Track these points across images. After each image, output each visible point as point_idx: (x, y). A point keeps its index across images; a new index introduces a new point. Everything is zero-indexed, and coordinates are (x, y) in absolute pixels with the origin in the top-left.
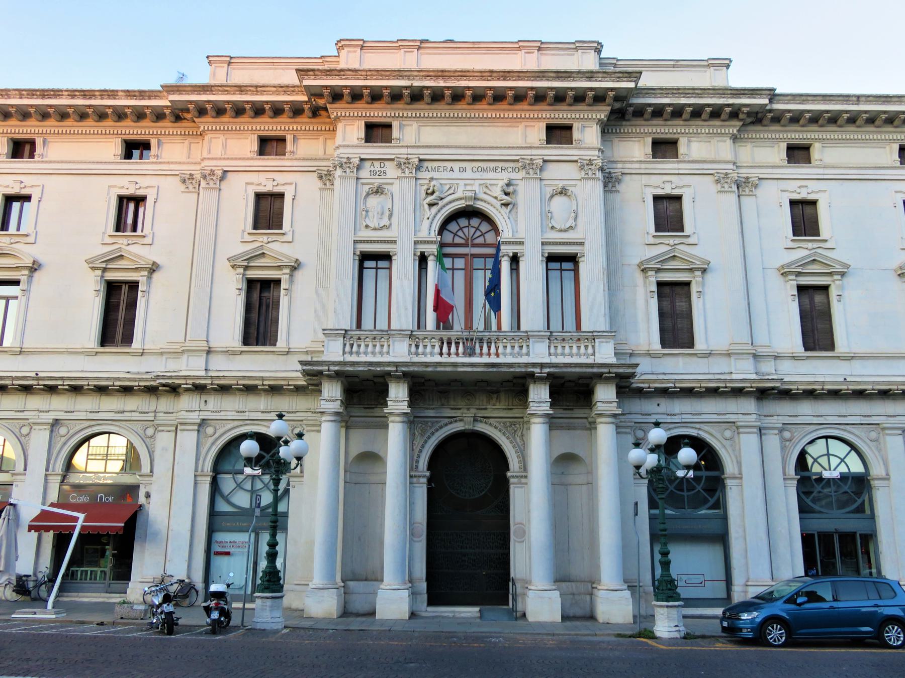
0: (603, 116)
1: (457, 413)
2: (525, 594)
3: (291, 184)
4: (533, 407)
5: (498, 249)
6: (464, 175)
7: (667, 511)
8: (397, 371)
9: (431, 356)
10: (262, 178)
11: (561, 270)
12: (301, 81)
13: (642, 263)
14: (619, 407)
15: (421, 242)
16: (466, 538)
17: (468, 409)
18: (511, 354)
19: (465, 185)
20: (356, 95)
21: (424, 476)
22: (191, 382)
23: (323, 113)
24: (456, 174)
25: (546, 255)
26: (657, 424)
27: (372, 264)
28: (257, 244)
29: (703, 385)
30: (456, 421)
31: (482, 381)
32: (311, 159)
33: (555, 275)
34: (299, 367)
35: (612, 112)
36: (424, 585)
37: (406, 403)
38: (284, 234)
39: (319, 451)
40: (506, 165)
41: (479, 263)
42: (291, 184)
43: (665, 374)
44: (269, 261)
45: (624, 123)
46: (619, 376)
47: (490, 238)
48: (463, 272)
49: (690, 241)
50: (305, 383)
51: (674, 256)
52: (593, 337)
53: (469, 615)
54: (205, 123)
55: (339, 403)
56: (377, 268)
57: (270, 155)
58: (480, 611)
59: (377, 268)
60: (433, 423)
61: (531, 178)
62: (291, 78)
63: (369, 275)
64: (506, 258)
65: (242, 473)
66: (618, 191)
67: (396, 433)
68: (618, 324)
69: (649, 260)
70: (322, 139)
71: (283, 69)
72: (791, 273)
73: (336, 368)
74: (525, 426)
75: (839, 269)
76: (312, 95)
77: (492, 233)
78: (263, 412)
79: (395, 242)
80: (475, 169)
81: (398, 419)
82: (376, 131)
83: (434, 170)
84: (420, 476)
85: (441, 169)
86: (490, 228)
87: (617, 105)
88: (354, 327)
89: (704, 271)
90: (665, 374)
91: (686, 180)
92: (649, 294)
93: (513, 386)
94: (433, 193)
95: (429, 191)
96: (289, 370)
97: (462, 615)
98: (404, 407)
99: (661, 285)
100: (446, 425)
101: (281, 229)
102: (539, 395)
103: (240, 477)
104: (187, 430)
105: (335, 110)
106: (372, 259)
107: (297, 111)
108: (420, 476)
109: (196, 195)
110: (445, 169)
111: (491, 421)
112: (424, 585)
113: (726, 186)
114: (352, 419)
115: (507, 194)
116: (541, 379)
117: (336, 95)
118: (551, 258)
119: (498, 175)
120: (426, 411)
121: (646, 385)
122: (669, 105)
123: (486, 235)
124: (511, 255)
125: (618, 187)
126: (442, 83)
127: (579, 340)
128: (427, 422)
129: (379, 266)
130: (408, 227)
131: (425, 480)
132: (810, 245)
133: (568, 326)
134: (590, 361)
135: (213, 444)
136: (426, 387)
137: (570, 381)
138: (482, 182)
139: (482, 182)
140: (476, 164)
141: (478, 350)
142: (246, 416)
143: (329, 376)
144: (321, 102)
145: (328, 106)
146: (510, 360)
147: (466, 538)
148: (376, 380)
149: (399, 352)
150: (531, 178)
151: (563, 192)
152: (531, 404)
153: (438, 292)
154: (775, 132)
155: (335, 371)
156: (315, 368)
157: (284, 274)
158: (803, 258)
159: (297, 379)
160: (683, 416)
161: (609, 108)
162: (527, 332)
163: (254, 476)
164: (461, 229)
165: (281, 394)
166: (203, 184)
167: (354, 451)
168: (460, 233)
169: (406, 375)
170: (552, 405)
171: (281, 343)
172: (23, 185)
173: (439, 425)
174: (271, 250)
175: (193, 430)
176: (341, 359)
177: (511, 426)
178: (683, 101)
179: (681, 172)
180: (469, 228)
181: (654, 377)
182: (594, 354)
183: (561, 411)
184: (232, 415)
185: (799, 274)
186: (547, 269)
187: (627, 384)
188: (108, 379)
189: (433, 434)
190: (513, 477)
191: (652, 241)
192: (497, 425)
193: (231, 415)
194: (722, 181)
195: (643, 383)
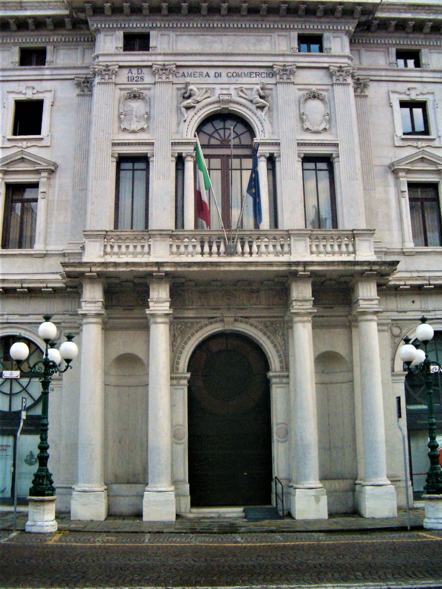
0: (351, 28)
2: (289, 494)
3: (51, 91)
4: (296, 307)
6: (219, 80)
7: (425, 407)
9: (192, 255)
10: (21, 87)
11: (316, 170)
13: (393, 164)
14: (379, 304)
15: (179, 143)
16: (232, 449)
19: (222, 89)
21: (185, 378)
23: (84, 27)
24: (212, 80)
25: (303, 155)
26: (423, 320)
27: (129, 166)
28: (15, 150)
30: (216, 322)
34: (61, 269)
35: (359, 25)
36: (187, 487)
37: (168, 304)
38: (42, 139)
39: (87, 351)
41: (235, 163)
42: (51, 91)
43: (418, 271)
44: (27, 165)
45: (370, 34)
47: (245, 139)
49: (436, 143)
50: (64, 285)
52: (353, 235)
53: (234, 515)
55: (100, 304)
56: (134, 170)
58: (244, 511)
59: (134, 170)
61: (285, 83)
63: (126, 176)
66: (366, 96)
69: (399, 162)
73: (99, 269)
74: (286, 325)
76: (73, 8)
77: (247, 135)
79: (152, 144)
80: (230, 75)
82: (136, 42)
83: (190, 75)
84: (181, 378)
85: (197, 75)
86: (245, 130)
87: (364, 19)
91: (430, 87)
93: (276, 286)
95: (186, 95)
97: (227, 515)
98: (165, 307)
99: (411, 185)
100: (206, 325)
101: (39, 133)
102: (302, 293)
106: (132, 163)
107: (58, 23)
108: (181, 378)
110: (201, 75)
111: (252, 321)
112: (188, 486)
114: (110, 320)
115: (261, 97)
116: (304, 278)
118: (307, 159)
122: (412, 20)
123: (241, 137)
124: (268, 155)
127: (339, 238)
130: (168, 129)
131: (185, 382)
134: (351, 258)
136: (184, 286)
140: (232, 70)
141: (239, 249)
143: (91, 278)
144: (82, 16)
147: (232, 449)
149: (160, 253)
150: (285, 83)
151: (314, 96)
152: (294, 303)
153: (198, 194)
156: (77, 269)
157: (43, 177)
160: (437, 313)
161: (356, 22)
162: (288, 231)
164: (216, 131)
168: (216, 135)
170: (315, 303)
173: (199, 325)
174: (30, 154)
176: (102, 260)
178: (423, 16)
179: (424, 80)
181: (408, 275)
182: (354, 252)
183: (321, 310)
186: (303, 170)
188: (15, 281)
189: (193, 335)
190: (275, 377)
191: (401, 143)
195: (401, 280)
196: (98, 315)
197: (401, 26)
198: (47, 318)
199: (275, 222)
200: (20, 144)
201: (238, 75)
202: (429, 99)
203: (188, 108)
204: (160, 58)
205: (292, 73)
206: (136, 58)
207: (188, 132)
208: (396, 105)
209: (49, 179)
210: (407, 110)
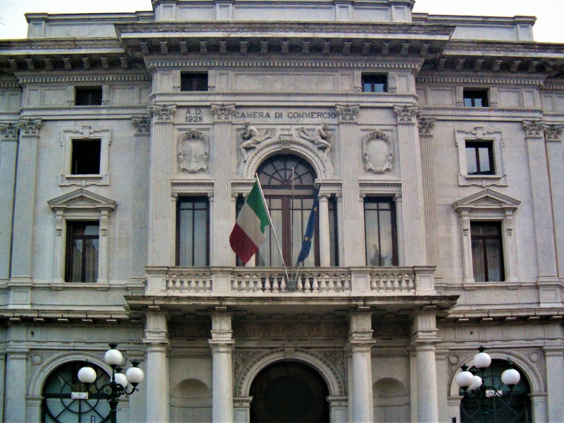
1: (279, 344)
5: (317, 191)
6: (280, 121)
8: (221, 305)
9: (253, 290)
10: (78, 126)
11: (193, 209)
12: (119, 35)
14: (438, 335)
17: (290, 340)
18: (203, 289)
19: (282, 130)
20: (174, 47)
21: (247, 401)
22: (19, 315)
23: (140, 66)
27: (189, 205)
29: (514, 314)
31: (304, 314)
32: (127, 108)
33: (373, 215)
34: (125, 302)
35: (426, 63)
37: (230, 335)
40: (323, 111)
46: (441, 308)
47: (306, 180)
48: (280, 212)
49: (501, 183)
50: (127, 317)
51: (82, 196)
52: (414, 272)
54: (22, 78)
55: (164, 334)
57: (86, 104)
60: (254, 353)
62: (110, 32)
63: (187, 215)
64: (324, 199)
65: (69, 396)
66: (431, 136)
67: (223, 363)
68: (438, 258)
70: (137, 89)
71: (98, 25)
72: (60, 209)
73: (162, 302)
75: (509, 205)
76: (129, 47)
78: (86, 343)
81: (158, 349)
82: (194, 81)
83: (249, 116)
84: (243, 401)
87: (431, 57)
88: (174, 264)
89: (112, 211)
90: (478, 305)
92: (462, 232)
94: (249, 138)
95: (246, 136)
96: (114, 306)
98: (228, 338)
100: (268, 355)
101: (98, 172)
103: (67, 401)
104: (17, 359)
105: (150, 62)
107: (113, 62)
108: (243, 401)
109: (16, 143)
111: (312, 350)
113: (30, 131)
114: (174, 349)
115: (323, 138)
117: (153, 47)
119: (316, 120)
120: (248, 342)
121: (462, 316)
124: (329, 196)
125: (432, 132)
126: (259, 35)
128: (249, 352)
129: (196, 207)
130: (229, 171)
131: (248, 404)
132: (484, 183)
133: (386, 261)
134: (411, 293)
135: (42, 371)
136: (244, 319)
137: (390, 313)
138: (299, 127)
139: (299, 127)
140: (293, 111)
141: (300, 285)
142: (71, 346)
144: (138, 54)
145: (145, 58)
146: (332, 294)
148: (199, 314)
150: (348, 123)
151: (378, 137)
152: (354, 335)
154: (450, 77)
155: (160, 305)
156: (141, 302)
157: (103, 215)
158: (477, 195)
159: (120, 313)
162: (349, 268)
163: (80, 400)
164: (277, 171)
165: (54, 327)
166: (22, 133)
167: (179, 380)
169: (230, 308)
170: (375, 335)
171: (102, 281)
172: (92, 131)
173: (261, 354)
175: (22, 359)
176: (165, 294)
177: (332, 354)
180: (292, 171)
184: (58, 346)
185: (66, 210)
186: (365, 210)
187: (444, 315)
190: (334, 400)
191: (67, 183)
192: (318, 354)
193: (56, 346)
194: (28, 127)
196: (162, 344)
197: (470, 63)
198: (113, 346)
199: (336, 260)
200: (79, 183)
201: (299, 116)
202: (496, 138)
203: (248, 149)
204: (218, 98)
205: (355, 113)
206: (193, 98)
207: (249, 173)
208: (462, 145)
209: (109, 217)
210: (473, 149)
